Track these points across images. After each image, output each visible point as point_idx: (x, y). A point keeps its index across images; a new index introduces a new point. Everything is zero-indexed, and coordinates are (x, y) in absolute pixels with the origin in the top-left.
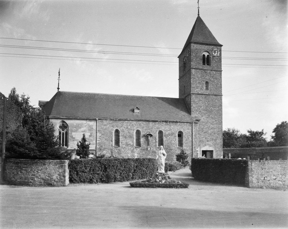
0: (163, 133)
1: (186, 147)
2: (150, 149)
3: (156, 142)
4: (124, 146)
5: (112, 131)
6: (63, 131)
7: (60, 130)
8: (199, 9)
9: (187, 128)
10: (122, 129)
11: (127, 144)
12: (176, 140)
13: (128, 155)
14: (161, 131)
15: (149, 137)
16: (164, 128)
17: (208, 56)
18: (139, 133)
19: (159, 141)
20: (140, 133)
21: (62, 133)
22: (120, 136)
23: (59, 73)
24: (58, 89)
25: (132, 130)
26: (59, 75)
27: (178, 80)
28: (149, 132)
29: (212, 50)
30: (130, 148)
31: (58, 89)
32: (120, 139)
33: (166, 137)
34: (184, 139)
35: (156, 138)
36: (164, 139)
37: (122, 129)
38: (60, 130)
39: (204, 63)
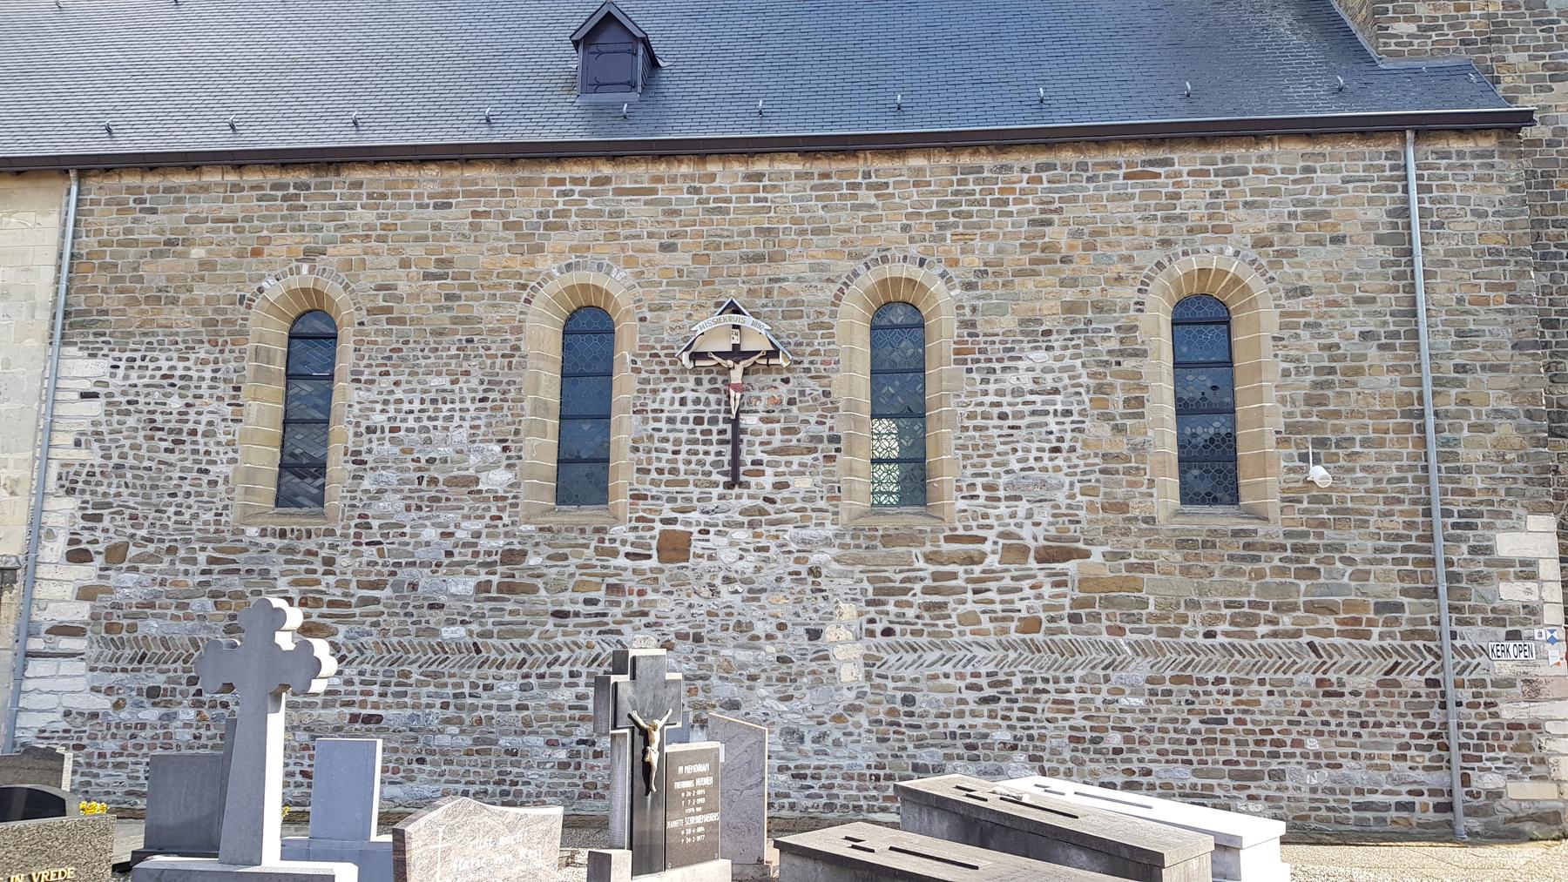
12: (1136, 404)
37: (380, 288)
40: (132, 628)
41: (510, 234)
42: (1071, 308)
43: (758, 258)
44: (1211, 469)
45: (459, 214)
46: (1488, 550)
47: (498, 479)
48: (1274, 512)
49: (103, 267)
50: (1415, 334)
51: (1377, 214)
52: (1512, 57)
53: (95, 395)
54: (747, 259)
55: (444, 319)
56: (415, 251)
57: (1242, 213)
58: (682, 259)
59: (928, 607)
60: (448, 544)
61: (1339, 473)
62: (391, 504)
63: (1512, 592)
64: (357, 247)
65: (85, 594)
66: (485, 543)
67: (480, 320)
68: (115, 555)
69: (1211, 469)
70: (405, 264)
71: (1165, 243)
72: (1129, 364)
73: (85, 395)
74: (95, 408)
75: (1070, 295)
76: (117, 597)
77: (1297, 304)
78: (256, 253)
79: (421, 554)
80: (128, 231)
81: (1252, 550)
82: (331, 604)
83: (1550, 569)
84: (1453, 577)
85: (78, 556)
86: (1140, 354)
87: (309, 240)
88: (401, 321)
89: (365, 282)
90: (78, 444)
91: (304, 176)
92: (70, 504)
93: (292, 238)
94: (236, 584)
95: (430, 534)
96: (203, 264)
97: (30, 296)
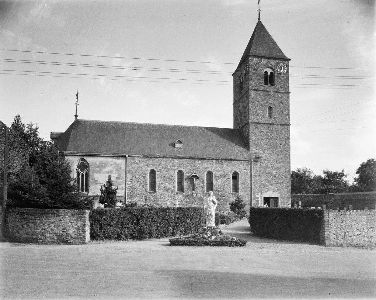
0: (213, 174)
1: (243, 193)
2: (195, 195)
3: (204, 185)
4: (162, 191)
5: (146, 171)
6: (83, 172)
7: (79, 170)
8: (259, 12)
9: (245, 167)
10: (160, 169)
11: (166, 189)
12: (229, 183)
13: (167, 203)
14: (210, 171)
15: (195, 179)
16: (214, 167)
17: (271, 73)
18: (182, 174)
19: (208, 184)
20: (182, 174)
21: (80, 174)
22: (157, 178)
23: (77, 95)
24: (76, 116)
25: (172, 170)
26: (77, 98)
27: (233, 105)
28: (195, 173)
29: (277, 65)
30: (169, 194)
31: (76, 116)
32: (157, 183)
33: (217, 180)
34: (240, 182)
35: (203, 181)
36: (214, 182)
37: (160, 169)
38: (78, 171)
39: (266, 83)
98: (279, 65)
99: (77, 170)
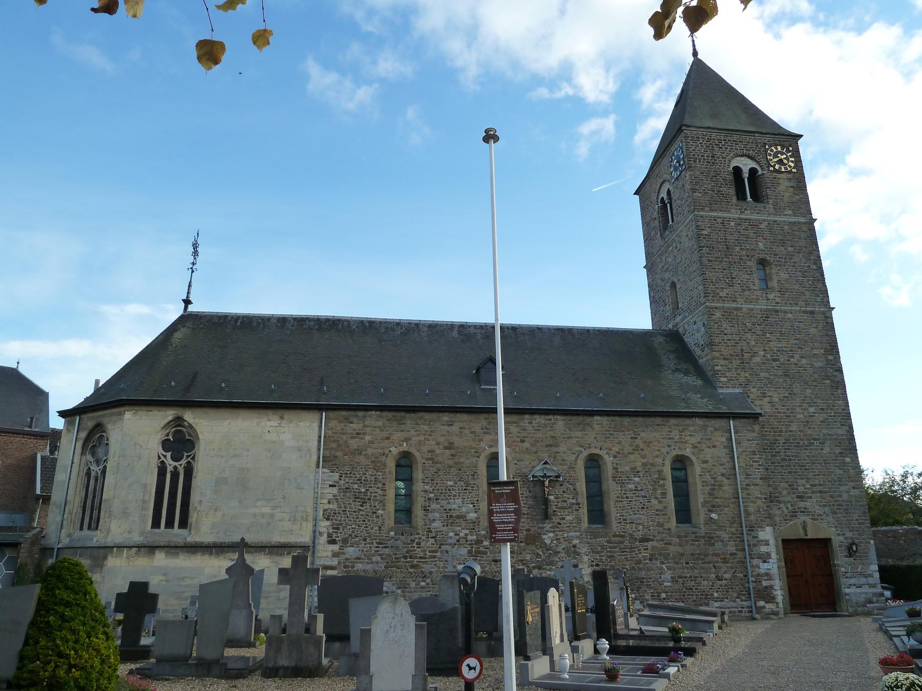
5: (383, 459)
6: (176, 464)
7: (165, 456)
8: (693, 41)
10: (429, 452)
11: (451, 516)
12: (664, 494)
17: (753, 171)
19: (589, 497)
21: (169, 469)
23: (195, 246)
24: (187, 302)
26: (195, 253)
29: (766, 150)
31: (187, 302)
33: (622, 484)
37: (429, 452)
38: (163, 459)
39: (741, 196)
40: (353, 567)
41: (472, 435)
42: (644, 465)
43: (551, 446)
44: (684, 513)
45: (455, 428)
46: (757, 537)
47: (473, 515)
48: (702, 527)
49: (334, 441)
50: (735, 475)
51: (723, 439)
52: (752, 390)
53: (334, 486)
54: (547, 446)
55: (451, 462)
56: (442, 439)
57: (688, 438)
58: (527, 445)
59: (609, 557)
60: (457, 537)
61: (719, 515)
62: (437, 525)
63: (764, 549)
64: (422, 438)
65: (335, 555)
66: (469, 537)
67: (463, 463)
68: (345, 541)
69: (684, 513)
70: (438, 444)
71: (669, 446)
72: (661, 482)
73: (330, 486)
74: (335, 491)
75: (644, 461)
76: (347, 556)
77: (705, 465)
78: (388, 438)
79: (450, 541)
80: (342, 429)
81: (697, 538)
82: (421, 558)
83: (772, 542)
84: (749, 545)
85: (332, 542)
86: (664, 479)
87: (406, 435)
88: (437, 463)
89: (425, 449)
90: (329, 503)
91: (403, 414)
92: (328, 523)
93: (400, 434)
94: (387, 551)
95: (451, 534)
96: (370, 442)
97: (309, 450)
98: (772, 151)
99: (159, 458)
